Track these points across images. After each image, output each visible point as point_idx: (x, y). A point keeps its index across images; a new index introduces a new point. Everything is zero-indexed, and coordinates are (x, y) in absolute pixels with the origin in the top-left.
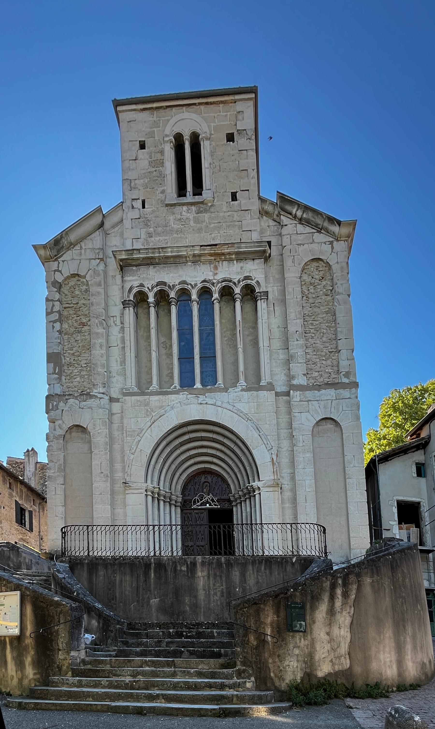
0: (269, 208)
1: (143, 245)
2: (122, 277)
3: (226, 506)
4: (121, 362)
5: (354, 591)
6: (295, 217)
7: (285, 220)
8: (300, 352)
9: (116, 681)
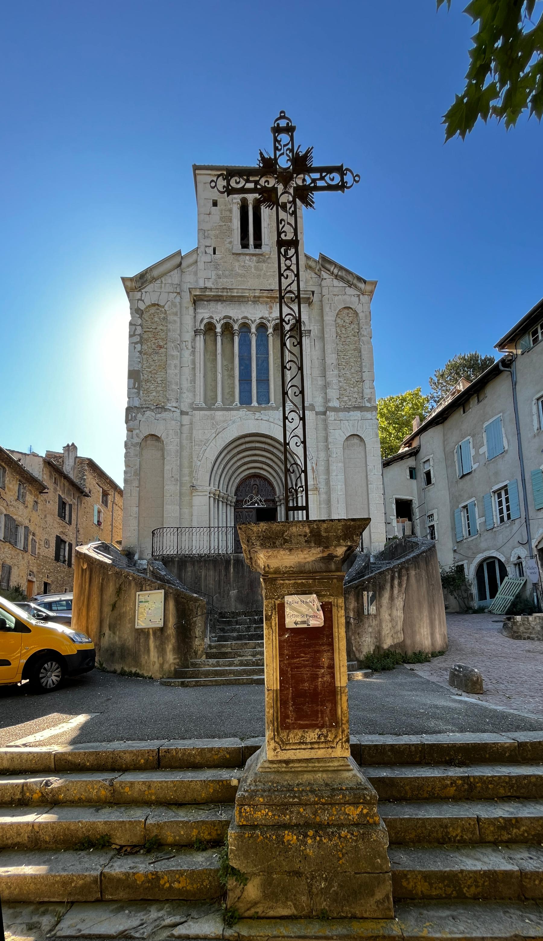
0: (313, 264)
1: (213, 284)
2: (195, 309)
3: (271, 505)
4: (191, 380)
5: (405, 582)
6: (333, 273)
7: (324, 275)
8: (335, 380)
9: (246, 660)
